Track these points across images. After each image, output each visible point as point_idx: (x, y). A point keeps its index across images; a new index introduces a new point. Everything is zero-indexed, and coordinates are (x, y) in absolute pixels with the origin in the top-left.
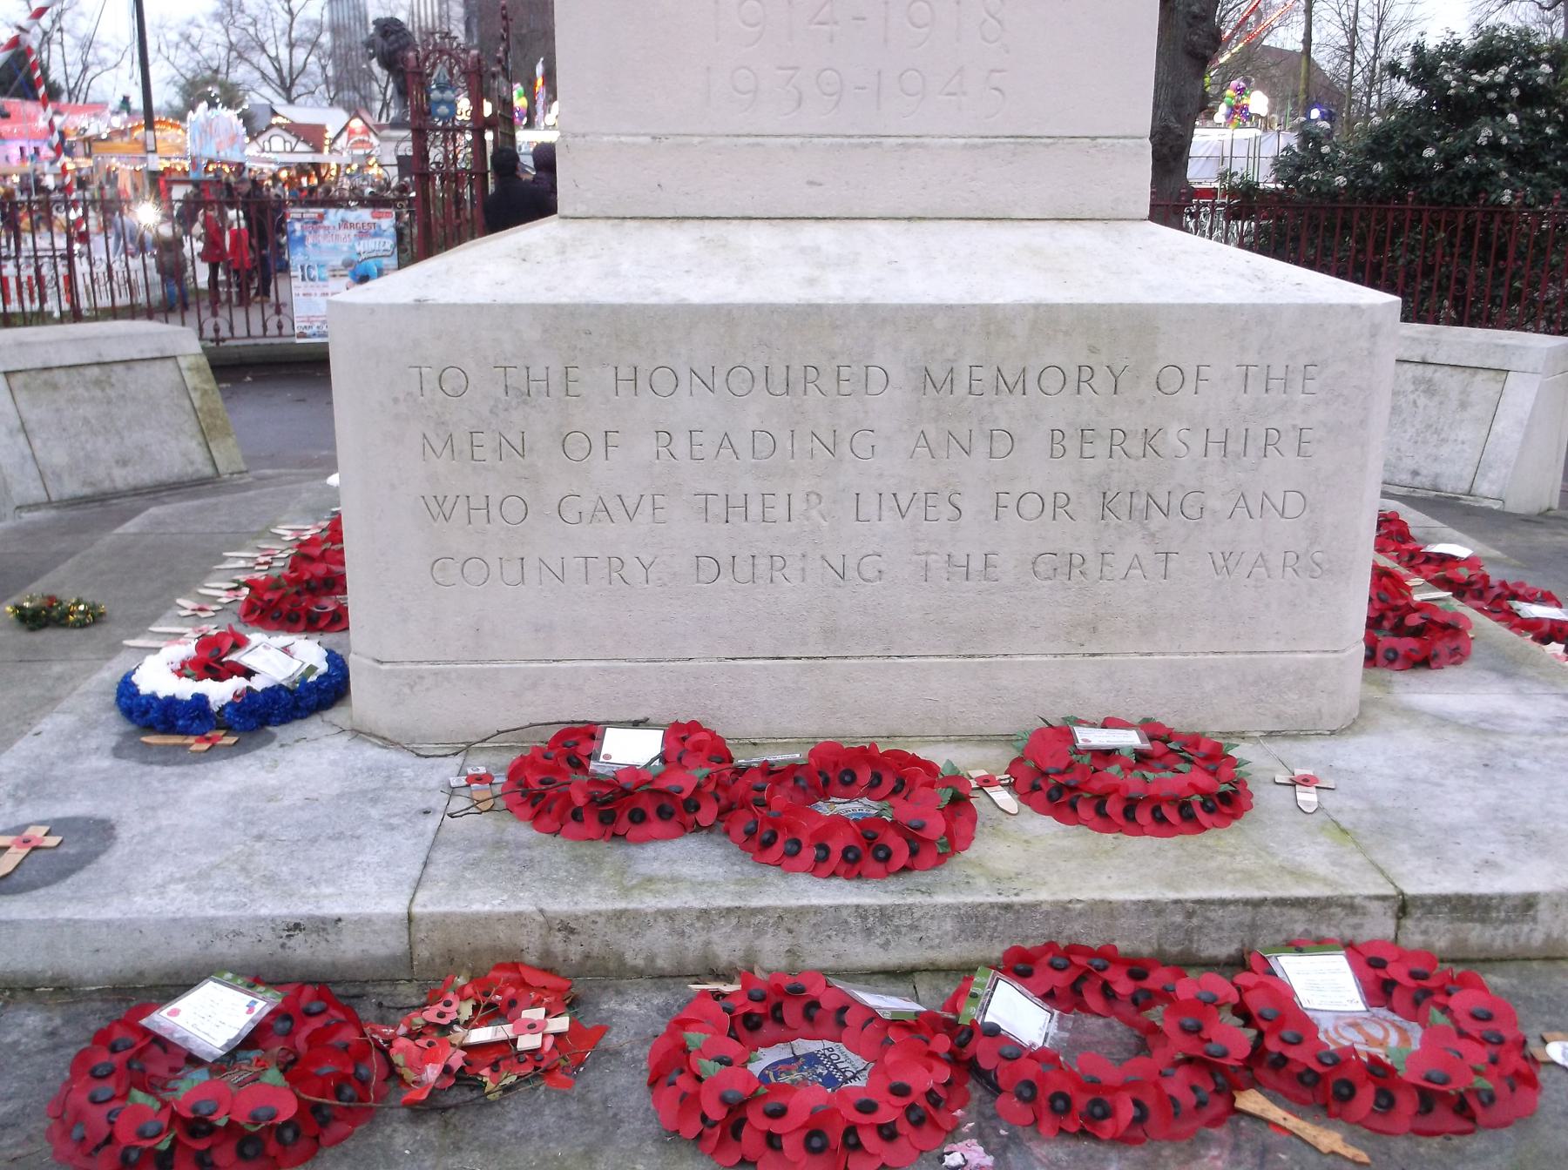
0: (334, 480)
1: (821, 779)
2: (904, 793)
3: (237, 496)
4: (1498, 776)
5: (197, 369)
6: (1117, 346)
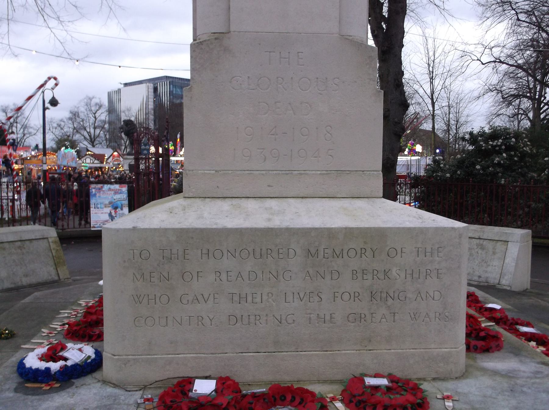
0: (101, 283)
1: (273, 399)
2: (303, 405)
3: (67, 288)
4: (516, 395)
5: (55, 242)
6: (374, 240)
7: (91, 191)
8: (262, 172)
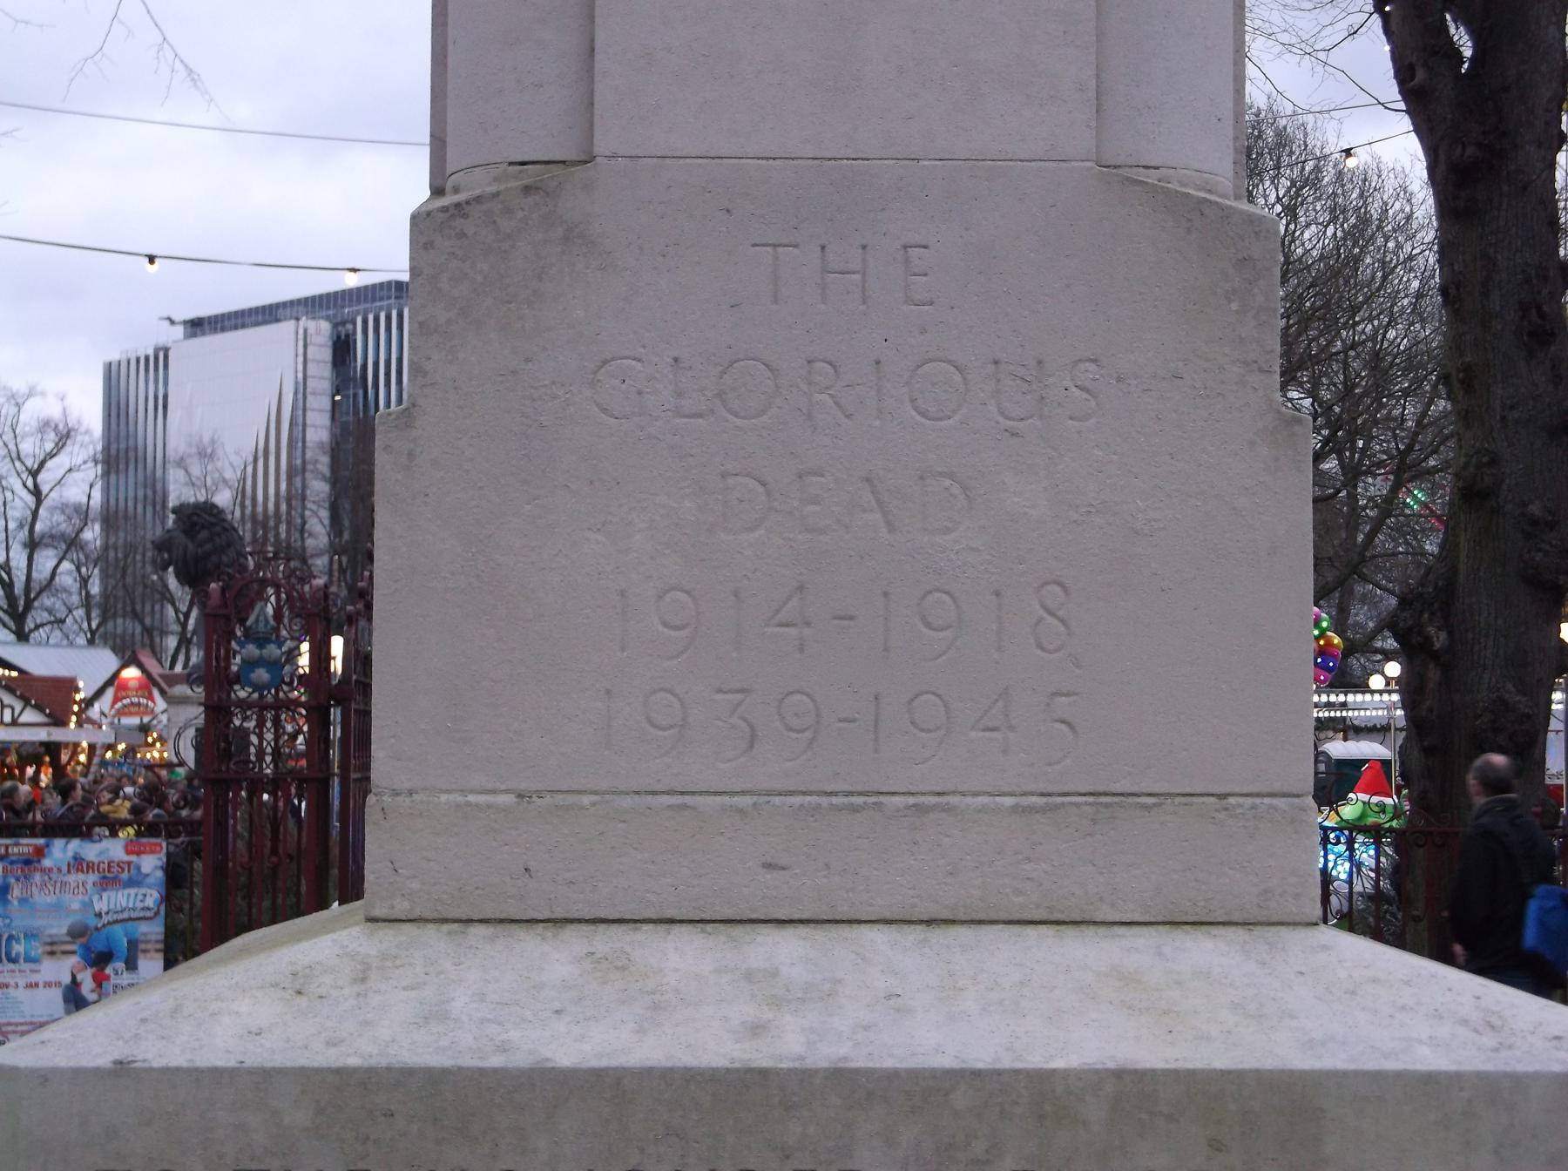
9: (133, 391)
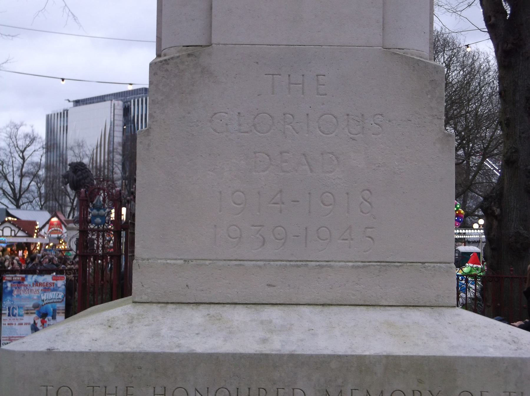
7: (4, 286)
8: (259, 263)
9: (56, 124)
